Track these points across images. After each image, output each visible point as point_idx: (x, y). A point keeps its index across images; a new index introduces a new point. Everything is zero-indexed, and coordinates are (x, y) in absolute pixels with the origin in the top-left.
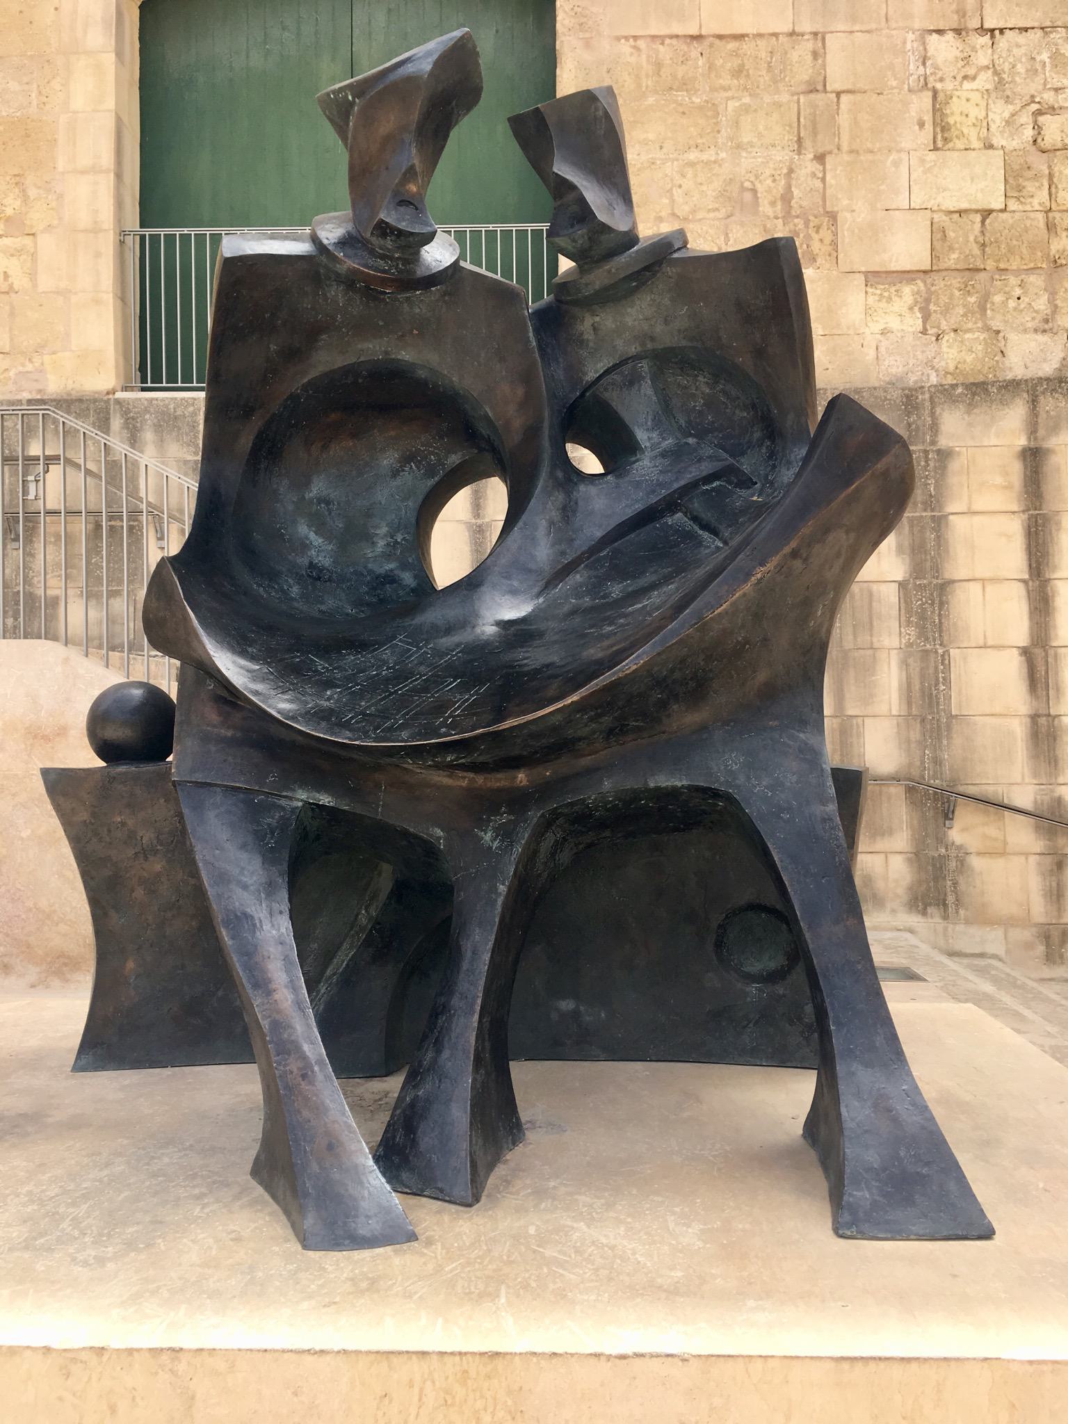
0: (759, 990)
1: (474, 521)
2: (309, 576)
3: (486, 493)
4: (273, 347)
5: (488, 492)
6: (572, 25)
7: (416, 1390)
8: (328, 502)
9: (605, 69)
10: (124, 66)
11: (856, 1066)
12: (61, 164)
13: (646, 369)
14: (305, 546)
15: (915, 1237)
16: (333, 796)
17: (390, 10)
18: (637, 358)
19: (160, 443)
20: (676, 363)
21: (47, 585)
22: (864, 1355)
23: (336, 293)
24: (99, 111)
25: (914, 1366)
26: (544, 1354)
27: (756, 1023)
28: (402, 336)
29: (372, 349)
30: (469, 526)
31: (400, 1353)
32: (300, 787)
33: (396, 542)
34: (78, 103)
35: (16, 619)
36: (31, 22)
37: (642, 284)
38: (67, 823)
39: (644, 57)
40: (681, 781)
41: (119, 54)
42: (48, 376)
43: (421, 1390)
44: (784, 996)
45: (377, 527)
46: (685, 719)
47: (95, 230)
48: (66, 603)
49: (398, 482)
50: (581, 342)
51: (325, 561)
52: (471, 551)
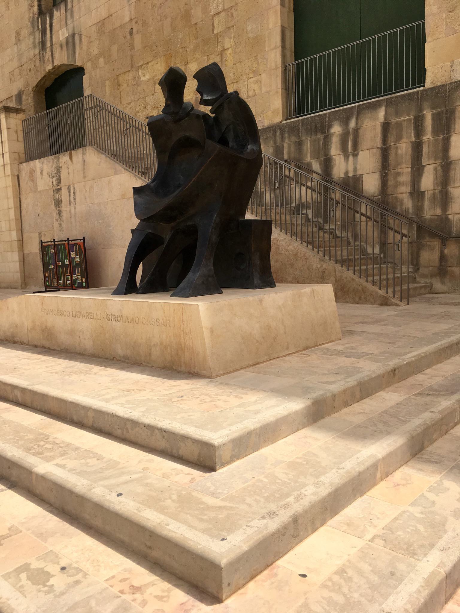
1: (383, 147)
19: (289, 137)
21: (23, 262)
34: (271, 26)
35: (254, 199)
42: (265, 121)
48: (265, 194)
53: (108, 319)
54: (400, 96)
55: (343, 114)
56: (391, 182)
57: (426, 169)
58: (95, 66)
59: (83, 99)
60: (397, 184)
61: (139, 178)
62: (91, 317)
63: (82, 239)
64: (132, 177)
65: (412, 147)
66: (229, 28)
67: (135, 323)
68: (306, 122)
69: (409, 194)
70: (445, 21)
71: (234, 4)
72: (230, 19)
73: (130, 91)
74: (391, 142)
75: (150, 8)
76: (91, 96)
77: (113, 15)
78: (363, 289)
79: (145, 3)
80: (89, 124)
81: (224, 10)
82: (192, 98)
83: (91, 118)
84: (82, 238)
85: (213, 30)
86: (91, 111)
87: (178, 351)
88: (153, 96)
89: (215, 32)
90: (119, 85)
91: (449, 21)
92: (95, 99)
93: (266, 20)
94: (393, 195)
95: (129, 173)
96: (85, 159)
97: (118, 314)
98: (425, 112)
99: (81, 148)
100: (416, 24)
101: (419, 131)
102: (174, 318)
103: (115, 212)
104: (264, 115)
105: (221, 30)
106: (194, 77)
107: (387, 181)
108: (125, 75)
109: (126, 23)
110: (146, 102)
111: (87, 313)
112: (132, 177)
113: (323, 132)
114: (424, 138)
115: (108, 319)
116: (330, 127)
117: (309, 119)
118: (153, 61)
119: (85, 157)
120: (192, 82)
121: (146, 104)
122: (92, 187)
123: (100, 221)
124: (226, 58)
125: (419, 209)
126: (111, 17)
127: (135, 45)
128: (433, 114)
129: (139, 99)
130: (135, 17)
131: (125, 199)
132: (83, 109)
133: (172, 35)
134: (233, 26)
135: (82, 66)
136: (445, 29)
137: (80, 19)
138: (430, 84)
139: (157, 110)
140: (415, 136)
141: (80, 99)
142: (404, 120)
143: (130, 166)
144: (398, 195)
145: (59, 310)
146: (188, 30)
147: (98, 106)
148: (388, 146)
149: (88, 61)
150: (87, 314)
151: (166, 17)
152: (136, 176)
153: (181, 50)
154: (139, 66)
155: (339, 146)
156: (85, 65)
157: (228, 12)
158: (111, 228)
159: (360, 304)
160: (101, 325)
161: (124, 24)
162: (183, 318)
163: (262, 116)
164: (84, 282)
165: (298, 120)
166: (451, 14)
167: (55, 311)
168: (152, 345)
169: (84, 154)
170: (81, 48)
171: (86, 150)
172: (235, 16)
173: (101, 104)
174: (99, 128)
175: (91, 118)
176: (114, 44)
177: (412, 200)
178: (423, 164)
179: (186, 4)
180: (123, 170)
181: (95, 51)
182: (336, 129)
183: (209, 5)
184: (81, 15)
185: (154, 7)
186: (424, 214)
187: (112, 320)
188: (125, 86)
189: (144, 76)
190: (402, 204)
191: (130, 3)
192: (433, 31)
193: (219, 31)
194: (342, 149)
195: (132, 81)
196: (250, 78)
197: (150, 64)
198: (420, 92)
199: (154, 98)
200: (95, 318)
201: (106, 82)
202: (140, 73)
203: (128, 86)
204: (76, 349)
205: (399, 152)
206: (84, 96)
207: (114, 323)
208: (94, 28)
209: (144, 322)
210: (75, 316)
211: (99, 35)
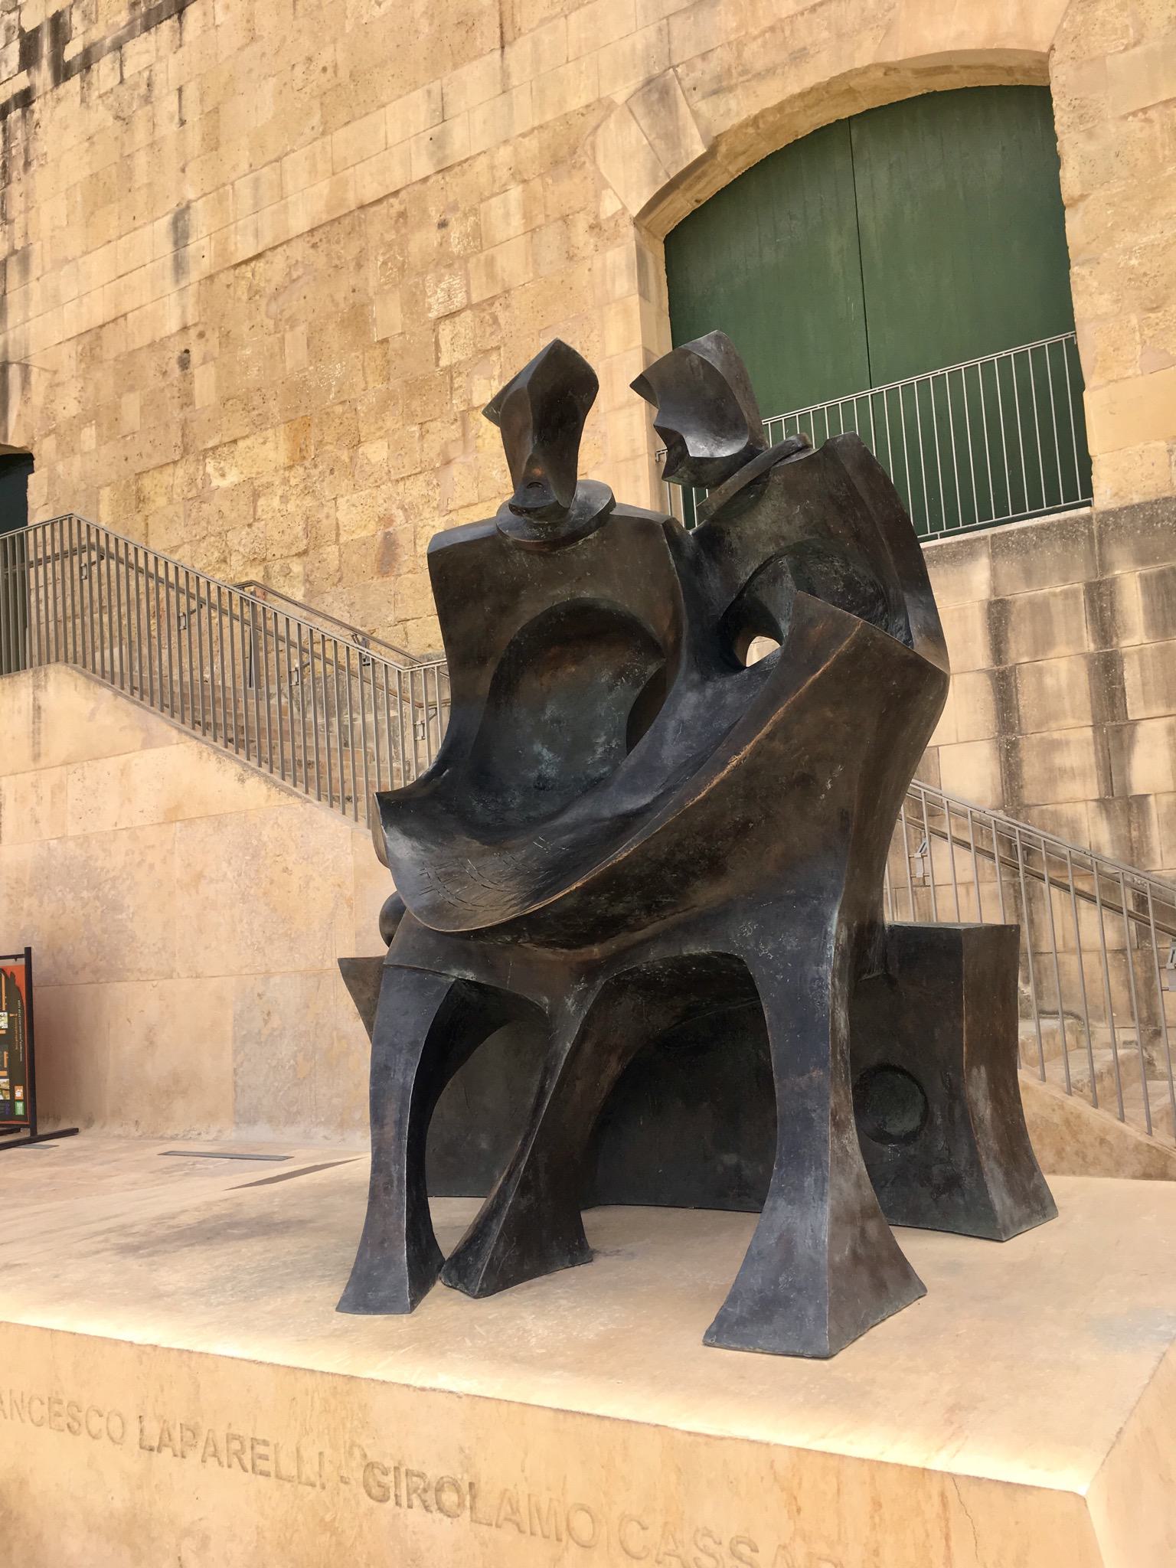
0: (893, 1149)
1: (995, 668)
2: (536, 787)
3: (1007, 636)
4: (488, 609)
5: (1009, 635)
6: (1070, 120)
7: (310, 1397)
8: (559, 722)
9: (1112, 154)
10: (649, 301)
11: (781, 1203)
13: (786, 564)
14: (538, 760)
15: (760, 1350)
16: (474, 972)
17: (891, 166)
18: (778, 556)
20: (811, 554)
22: (545, 1405)
23: (520, 558)
24: (630, 350)
25: (607, 1423)
26: (378, 1381)
27: (893, 1183)
28: (580, 579)
29: (562, 593)
30: (990, 673)
31: (301, 1369)
32: (455, 967)
33: (611, 748)
36: (571, 288)
37: (760, 496)
38: (357, 1002)
39: (1157, 127)
40: (705, 949)
41: (644, 294)
43: (312, 1398)
44: (914, 1156)
45: (598, 736)
46: (706, 895)
47: (634, 457)
49: (614, 695)
50: (733, 552)
51: (551, 772)
52: (995, 700)
53: (376, 1491)
54: (1033, 529)
56: (1031, 769)
57: (1142, 730)
58: (68, 448)
59: (27, 532)
60: (1054, 776)
61: (229, 757)
62: (262, 1465)
63: (20, 956)
64: (205, 754)
65: (1090, 670)
66: (486, 352)
67: (564, 1536)
69: (1094, 804)
70: (1138, 334)
71: (498, 291)
72: (489, 330)
73: (178, 517)
74: (1019, 651)
75: (245, 297)
76: (70, 519)
77: (130, 316)
78: (1067, 1122)
79: (228, 286)
80: (42, 607)
81: (469, 306)
82: (373, 536)
83: (50, 588)
84: (23, 952)
85: (438, 359)
86: (41, 569)
88: (249, 530)
89: (444, 363)
90: (141, 499)
91: (1151, 334)
92: (84, 529)
93: (596, 332)
94: (1044, 807)
95: (195, 742)
96: (43, 703)
97: (443, 1472)
98: (1117, 572)
99: (30, 672)
100: (1029, 349)
101: (1105, 623)
103: (140, 864)
105: (462, 358)
106: (640, 385)
107: (1019, 765)
108: (161, 473)
109: (169, 337)
110: (226, 544)
111: (231, 1438)
112: (205, 754)
114: (1124, 643)
115: (376, 1491)
118: (252, 438)
119: (40, 694)
120: (374, 491)
121: (227, 551)
122: (59, 788)
123: (85, 894)
124: (479, 430)
125: (1135, 850)
126: (121, 321)
127: (196, 393)
128: (1145, 579)
129: (204, 538)
130: (197, 320)
131: (178, 824)
132: (23, 561)
133: (311, 368)
134: (498, 348)
135: (26, 447)
136: (1142, 355)
137: (27, 324)
138: (1111, 498)
139: (261, 568)
140: (1093, 635)
141: (15, 532)
142: (1055, 595)
143: (195, 722)
144: (1059, 807)
145: (60, 1402)
146: (361, 357)
147: (91, 547)
148: (1011, 665)
149: (47, 435)
150: (235, 1445)
151: (292, 322)
152: (220, 750)
153: (339, 409)
154: (205, 450)
156: (36, 446)
157: (484, 310)
158: (124, 916)
159: (1063, 1173)
160: (328, 1518)
161: (161, 340)
164: (19, 1101)
166: (1152, 315)
167: (37, 1403)
169: (37, 687)
170: (26, 401)
171: (46, 675)
172: (502, 321)
173: (103, 543)
174: (74, 616)
175: (50, 588)
176: (131, 389)
177: (1109, 818)
178: (1130, 717)
179: (354, 291)
180: (174, 733)
181: (68, 406)
183: (424, 292)
184: (31, 314)
185: (257, 297)
186: (1153, 861)
187: (404, 1501)
188: (161, 501)
189: (223, 475)
190: (1075, 833)
191: (183, 284)
192: (1104, 360)
193: (454, 361)
195: (186, 489)
197: (241, 444)
198: (1094, 517)
199: (252, 536)
200: (284, 1473)
201: (102, 492)
202: (210, 469)
203: (170, 501)
205: (1049, 681)
206: (29, 525)
207: (415, 1516)
208: (69, 349)
209: (634, 1546)
210: (155, 1444)
211: (83, 366)
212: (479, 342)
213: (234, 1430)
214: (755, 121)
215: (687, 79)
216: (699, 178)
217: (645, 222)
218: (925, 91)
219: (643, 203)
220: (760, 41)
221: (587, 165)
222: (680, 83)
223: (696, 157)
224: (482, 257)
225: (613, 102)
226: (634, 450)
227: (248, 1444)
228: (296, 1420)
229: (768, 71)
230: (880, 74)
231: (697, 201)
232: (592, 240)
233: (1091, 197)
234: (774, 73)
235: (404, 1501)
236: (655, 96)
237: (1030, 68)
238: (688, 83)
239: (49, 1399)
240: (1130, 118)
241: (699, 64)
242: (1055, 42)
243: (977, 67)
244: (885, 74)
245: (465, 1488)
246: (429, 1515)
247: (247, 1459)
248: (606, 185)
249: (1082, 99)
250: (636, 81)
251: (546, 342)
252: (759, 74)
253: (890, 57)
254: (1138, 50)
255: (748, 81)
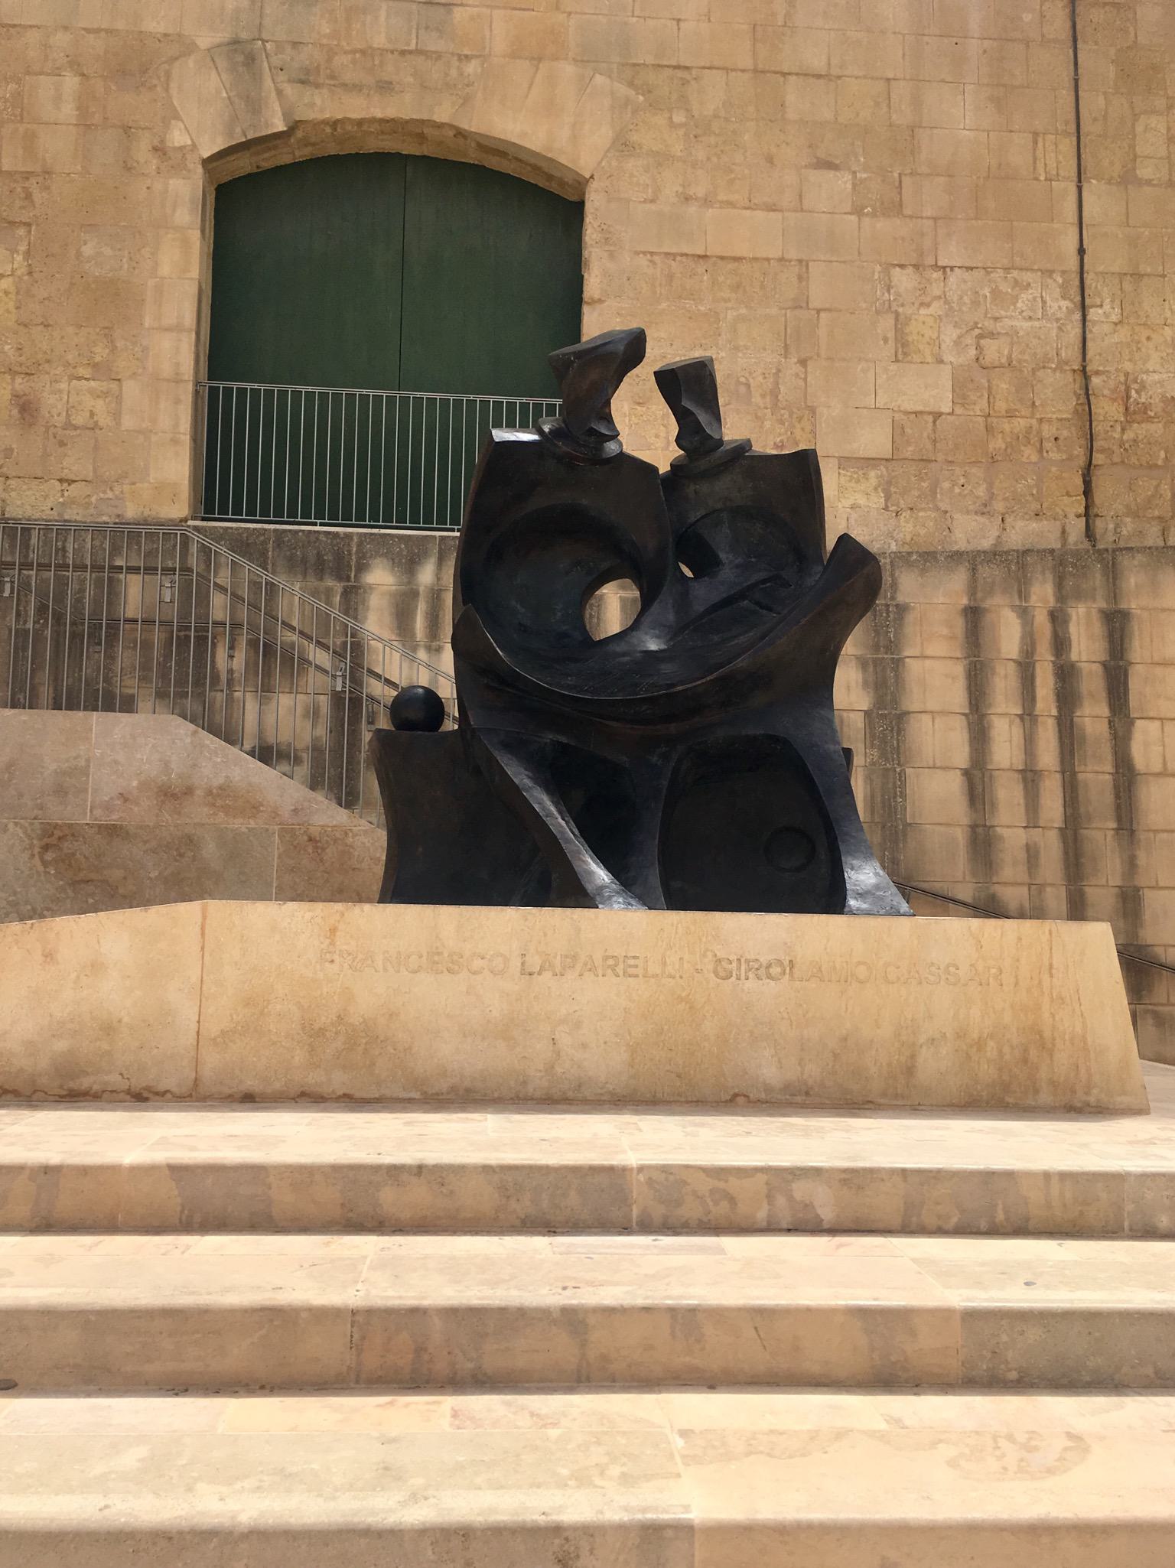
12: (148, 322)
34: (165, 270)
41: (203, 231)
47: (178, 381)
55: (400, 547)
62: (631, 971)
68: (289, 541)
87: (1026, 1050)
97: (772, 957)
98: (605, 591)
102: (1018, 960)
104: (126, 488)
113: (341, 573)
116: (362, 568)
117: (300, 534)
128: (622, 599)
134: (29, 225)
155: (388, 619)
162: (1051, 957)
163: (117, 489)
165: (265, 530)
166: (639, 408)
168: (922, 1041)
182: (381, 578)
187: (743, 976)
194: (399, 628)
196: (79, 378)
204: (525, 1083)
207: (751, 984)
212: (5, 211)
213: (609, 953)
214: (335, 124)
215: (275, 57)
216: (269, 149)
217: (210, 166)
218: (476, 162)
219: (216, 150)
220: (350, 57)
221: (159, 89)
222: (267, 58)
223: (275, 131)
224: (22, 128)
225: (194, 44)
226: (177, 374)
227: (621, 960)
228: (663, 941)
229: (355, 86)
230: (451, 133)
231: (258, 167)
232: (155, 161)
233: (607, 303)
234: (360, 90)
235: (743, 976)
236: (240, 58)
237: (568, 183)
238: (276, 61)
239: (428, 953)
240: (641, 255)
241: (289, 50)
242: (595, 174)
243: (527, 164)
244: (455, 136)
245: (786, 963)
246: (760, 982)
247: (620, 970)
248: (177, 117)
249: (609, 226)
250: (223, 36)
251: (698, 354)
252: (346, 85)
253: (465, 126)
254: (653, 207)
255: (334, 86)
